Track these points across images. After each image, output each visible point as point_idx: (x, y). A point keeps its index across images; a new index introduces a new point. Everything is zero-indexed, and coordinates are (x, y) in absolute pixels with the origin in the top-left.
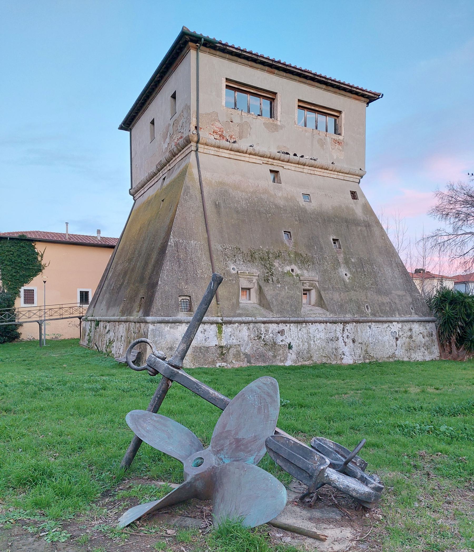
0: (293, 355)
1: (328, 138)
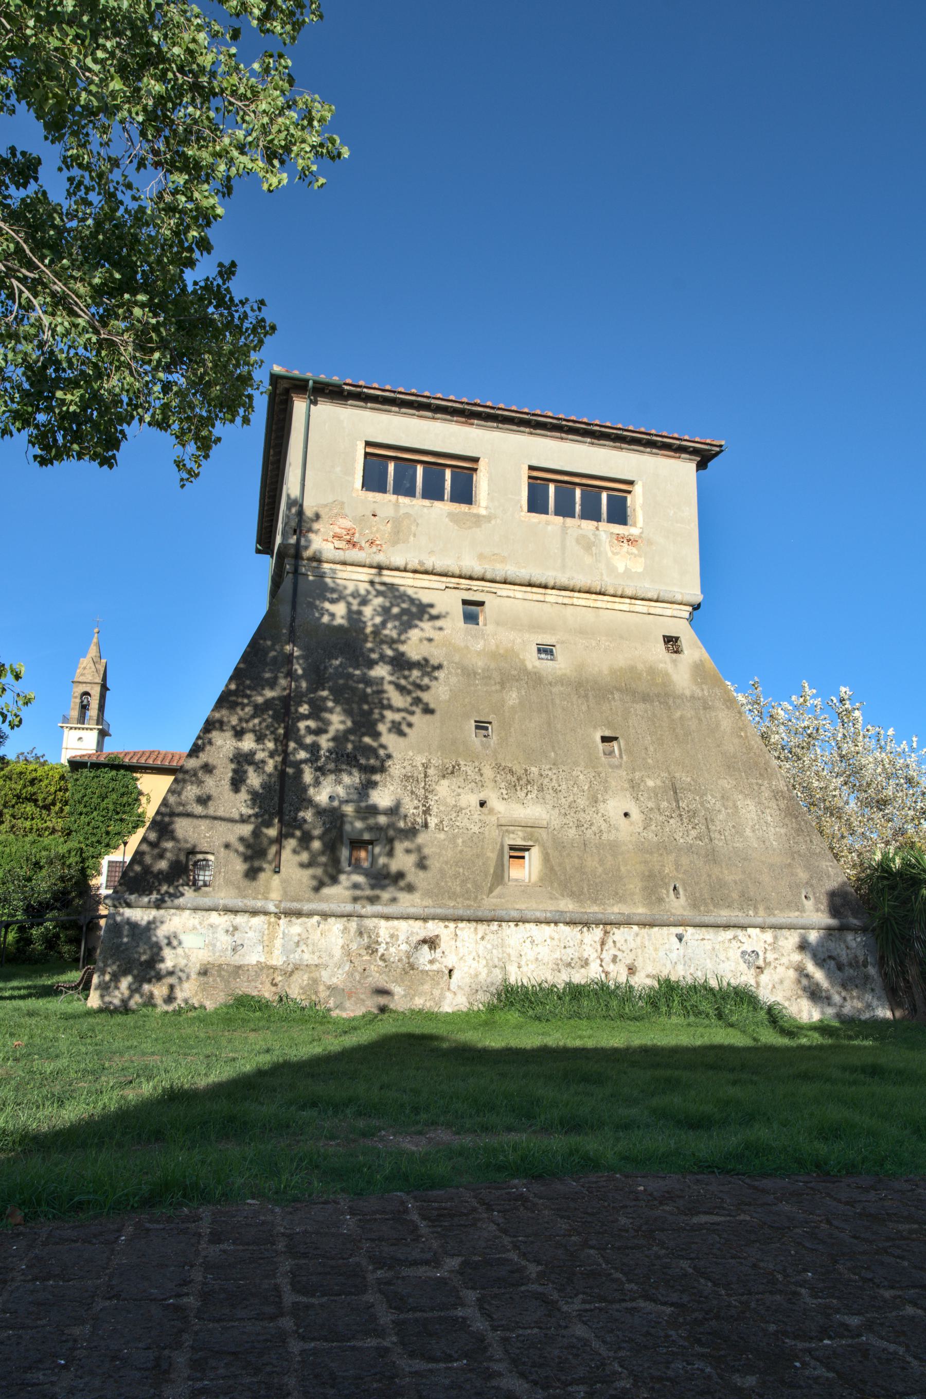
1: (602, 533)
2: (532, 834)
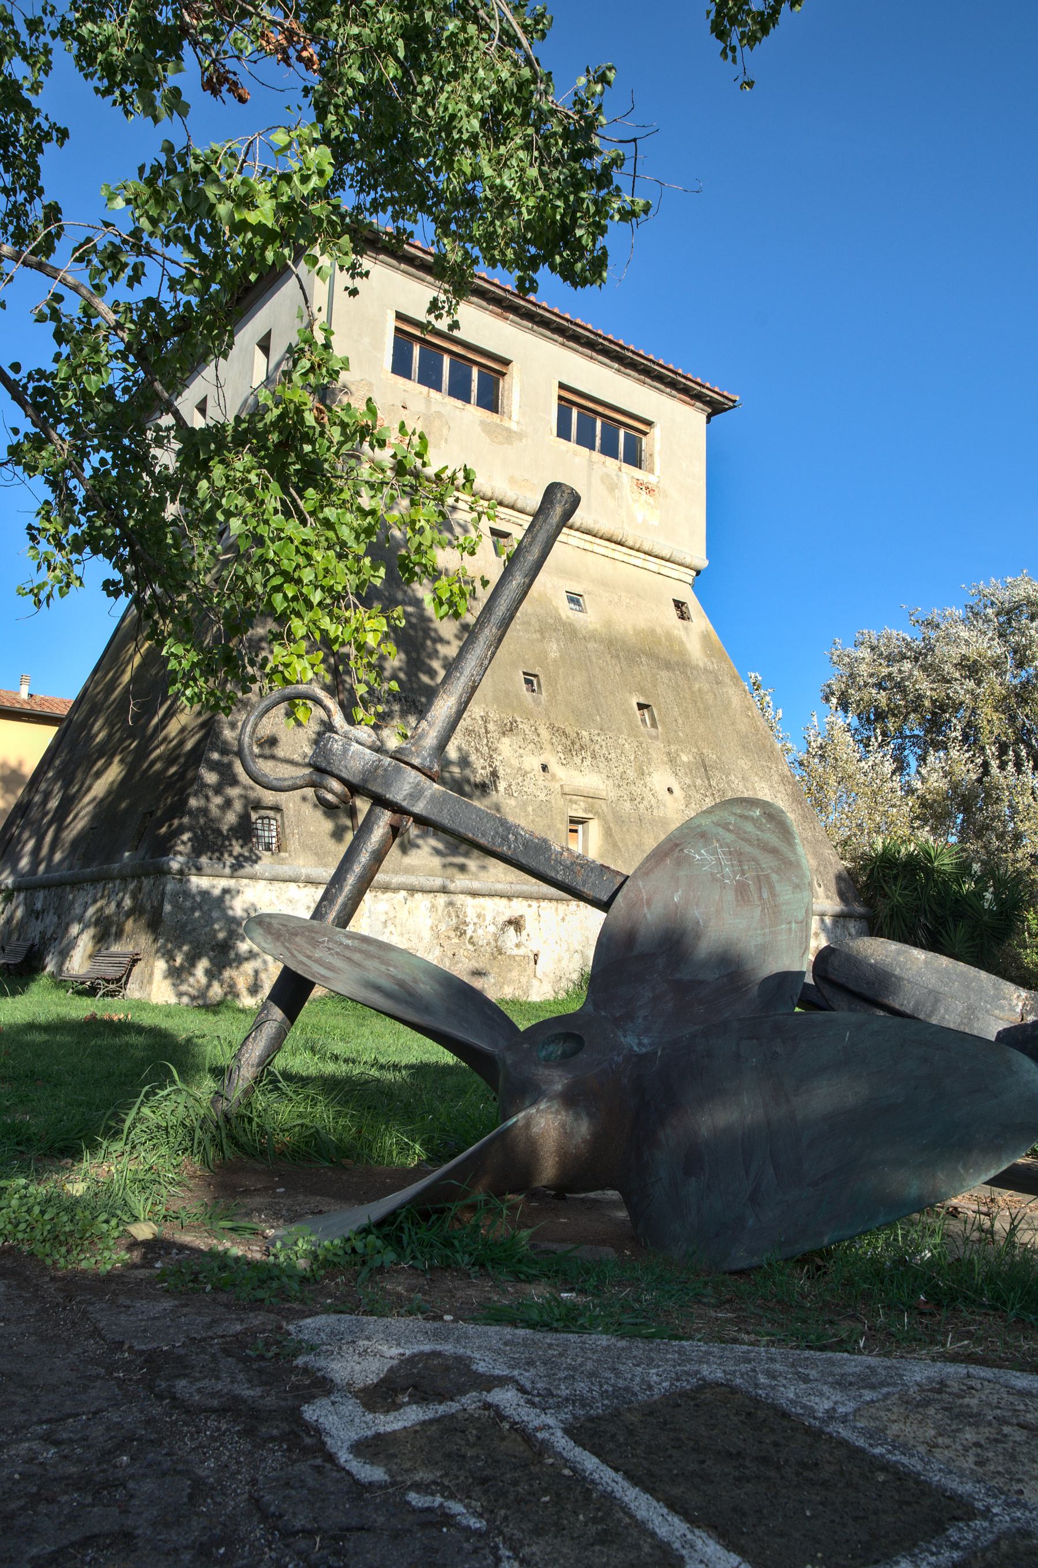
0: (545, 983)
2: (592, 806)
